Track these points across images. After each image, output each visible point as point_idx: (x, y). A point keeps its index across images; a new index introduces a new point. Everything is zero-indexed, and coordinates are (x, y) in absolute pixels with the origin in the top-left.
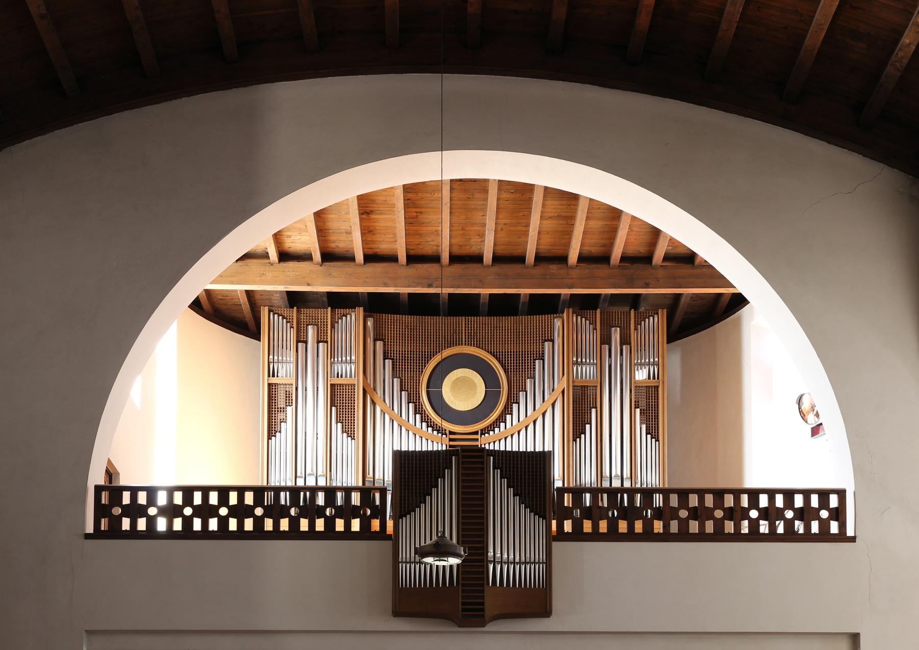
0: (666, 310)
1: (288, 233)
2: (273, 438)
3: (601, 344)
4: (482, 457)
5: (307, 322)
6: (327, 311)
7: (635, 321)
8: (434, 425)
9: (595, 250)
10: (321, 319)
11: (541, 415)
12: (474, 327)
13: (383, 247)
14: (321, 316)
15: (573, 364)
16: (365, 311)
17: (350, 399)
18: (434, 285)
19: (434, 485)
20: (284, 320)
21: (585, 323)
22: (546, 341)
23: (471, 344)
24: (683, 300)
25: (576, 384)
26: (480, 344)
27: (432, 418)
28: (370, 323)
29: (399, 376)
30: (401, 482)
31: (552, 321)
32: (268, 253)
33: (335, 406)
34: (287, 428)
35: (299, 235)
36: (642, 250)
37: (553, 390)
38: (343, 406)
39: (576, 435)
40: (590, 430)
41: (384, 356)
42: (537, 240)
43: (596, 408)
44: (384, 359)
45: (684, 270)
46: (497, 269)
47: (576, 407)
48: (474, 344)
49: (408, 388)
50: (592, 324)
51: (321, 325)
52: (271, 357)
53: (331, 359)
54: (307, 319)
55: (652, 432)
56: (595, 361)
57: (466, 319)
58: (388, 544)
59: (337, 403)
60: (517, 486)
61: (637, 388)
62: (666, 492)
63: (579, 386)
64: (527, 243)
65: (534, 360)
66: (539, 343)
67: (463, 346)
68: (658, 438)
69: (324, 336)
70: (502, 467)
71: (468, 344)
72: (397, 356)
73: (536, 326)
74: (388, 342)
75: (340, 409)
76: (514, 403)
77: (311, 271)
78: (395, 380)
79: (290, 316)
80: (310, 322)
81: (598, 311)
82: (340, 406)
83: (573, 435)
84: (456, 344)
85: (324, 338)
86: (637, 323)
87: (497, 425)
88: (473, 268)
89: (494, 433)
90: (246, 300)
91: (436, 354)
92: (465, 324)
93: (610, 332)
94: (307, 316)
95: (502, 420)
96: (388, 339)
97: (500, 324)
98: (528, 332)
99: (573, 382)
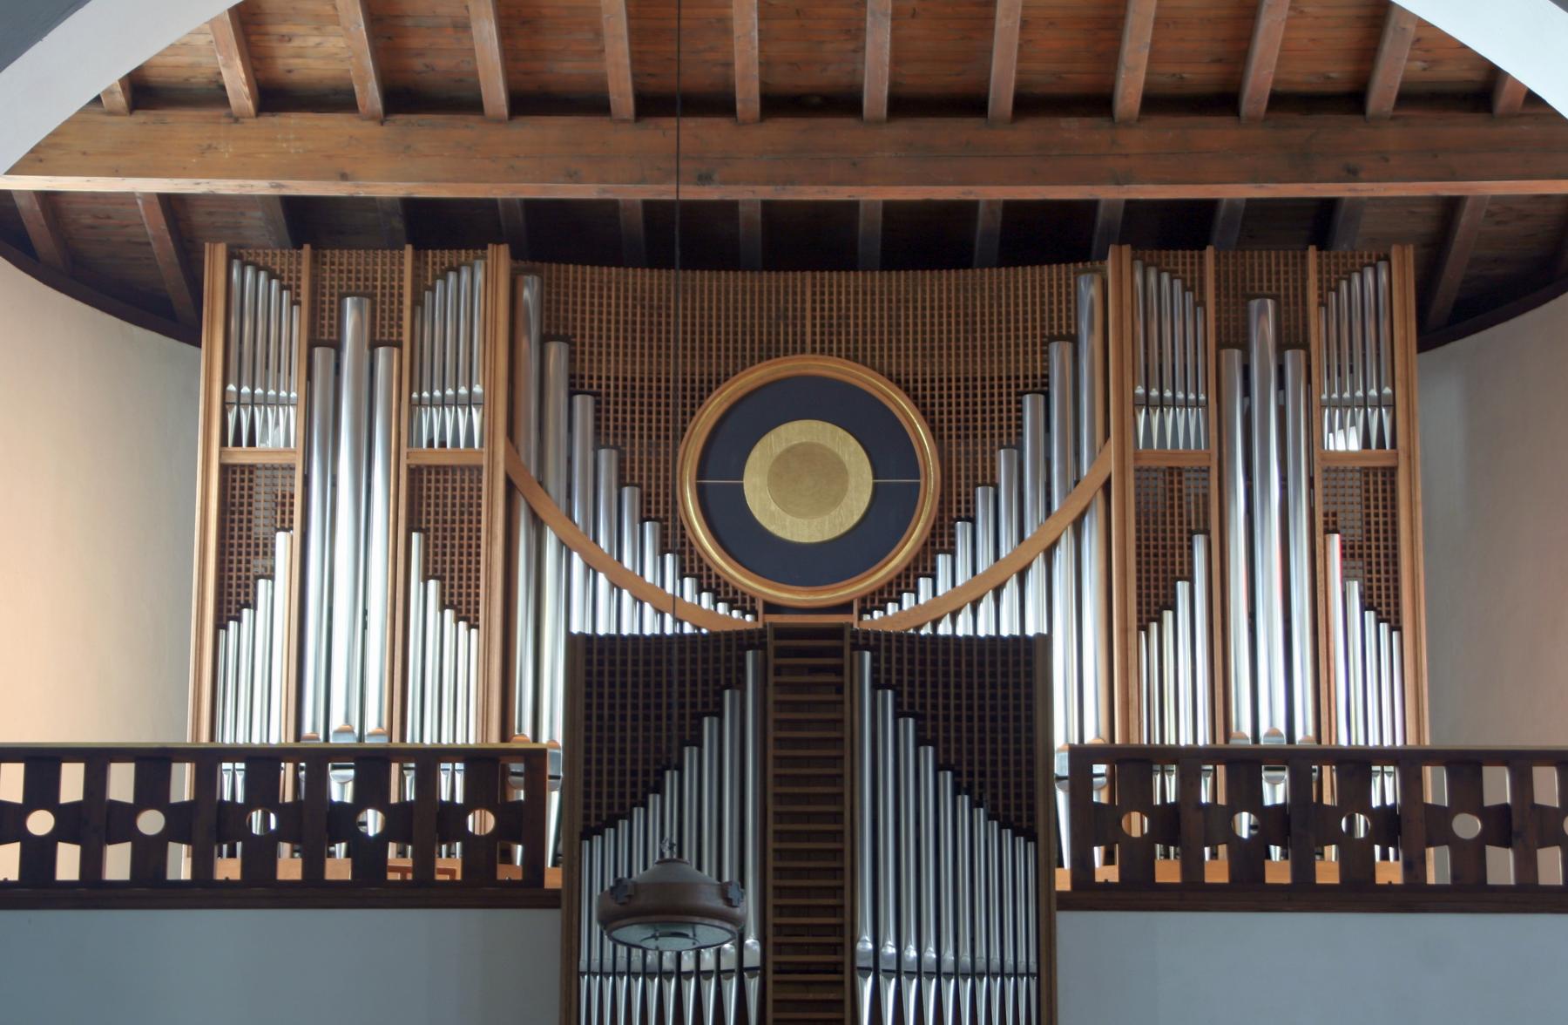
0: (1411, 246)
1: (284, 29)
2: (232, 625)
3: (1220, 346)
4: (838, 652)
5: (341, 287)
6: (402, 257)
7: (1320, 280)
8: (718, 585)
9: (1199, 74)
10: (384, 279)
11: (1041, 556)
12: (839, 301)
13: (567, 69)
14: (384, 271)
15: (1135, 405)
16: (515, 256)
17: (465, 509)
18: (716, 177)
19: (691, 736)
20: (274, 282)
21: (1169, 288)
22: (1053, 339)
23: (831, 350)
24: (1464, 219)
25: (1144, 463)
26: (856, 349)
27: (712, 565)
28: (528, 294)
29: (616, 443)
30: (588, 729)
31: (1072, 282)
32: (223, 88)
33: (419, 530)
34: (275, 595)
35: (315, 32)
36: (1335, 72)
37: (1077, 482)
38: (445, 530)
39: (1148, 612)
40: (1190, 598)
41: (572, 385)
42: (1020, 46)
43: (1207, 532)
44: (571, 394)
45: (1462, 128)
46: (903, 129)
47: (1147, 531)
48: (839, 349)
49: (641, 477)
50: (1192, 289)
51: (383, 295)
52: (232, 388)
53: (411, 394)
54: (341, 279)
55: (1380, 604)
56: (1202, 397)
57: (814, 278)
58: (547, 922)
59: (428, 522)
60: (947, 740)
61: (1329, 471)
62: (1408, 762)
63: (1156, 470)
64: (991, 52)
65: (1017, 394)
66: (1034, 344)
67: (808, 355)
68: (1398, 621)
69: (391, 327)
70: (900, 682)
71: (822, 350)
72: (608, 387)
73: (1025, 296)
74: (583, 345)
75: (436, 538)
76: (959, 519)
77: (351, 137)
78: (603, 453)
79: (290, 271)
80: (349, 287)
81: (1210, 252)
82: (436, 530)
83: (1139, 612)
84: (786, 350)
85: (391, 334)
86: (1328, 287)
87: (907, 585)
88: (833, 131)
89: (900, 608)
90: (163, 226)
91: (726, 380)
92: (814, 294)
93: (1246, 312)
94: (341, 271)
95: (925, 569)
96: (583, 336)
97: (915, 292)
98: (1000, 314)
99: (1137, 456)
